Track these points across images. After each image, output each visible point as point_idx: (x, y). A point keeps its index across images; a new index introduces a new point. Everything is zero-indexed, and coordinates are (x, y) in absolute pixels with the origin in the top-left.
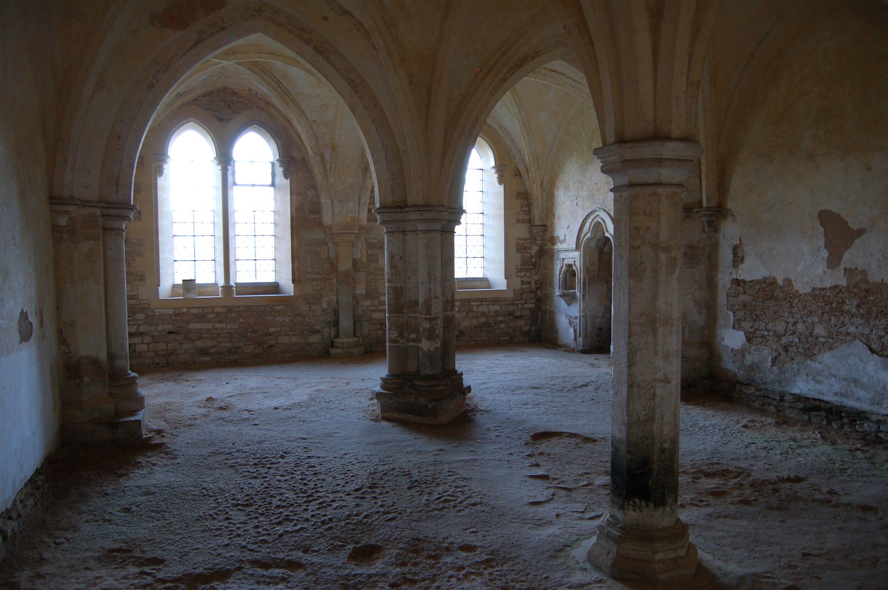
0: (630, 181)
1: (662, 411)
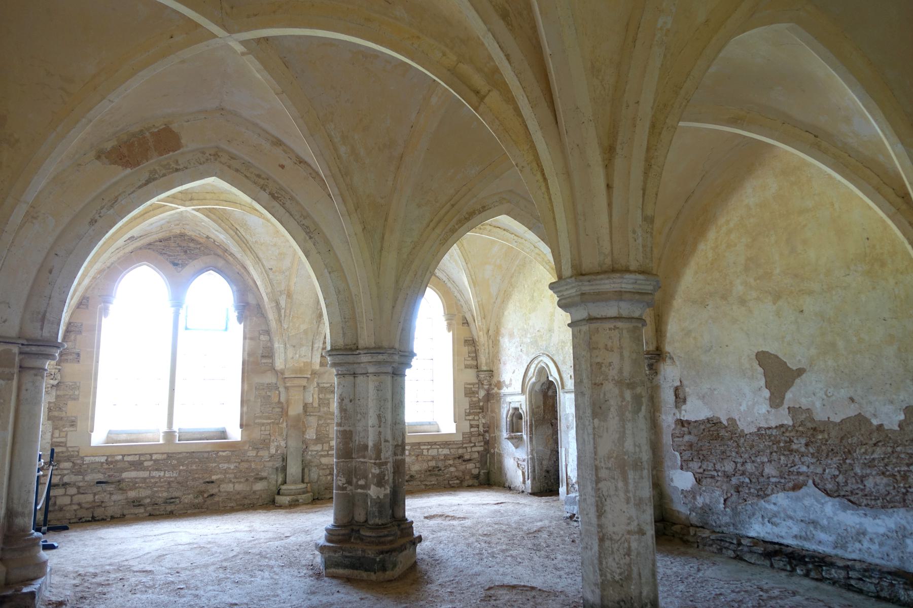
0: (589, 314)
1: (639, 568)
